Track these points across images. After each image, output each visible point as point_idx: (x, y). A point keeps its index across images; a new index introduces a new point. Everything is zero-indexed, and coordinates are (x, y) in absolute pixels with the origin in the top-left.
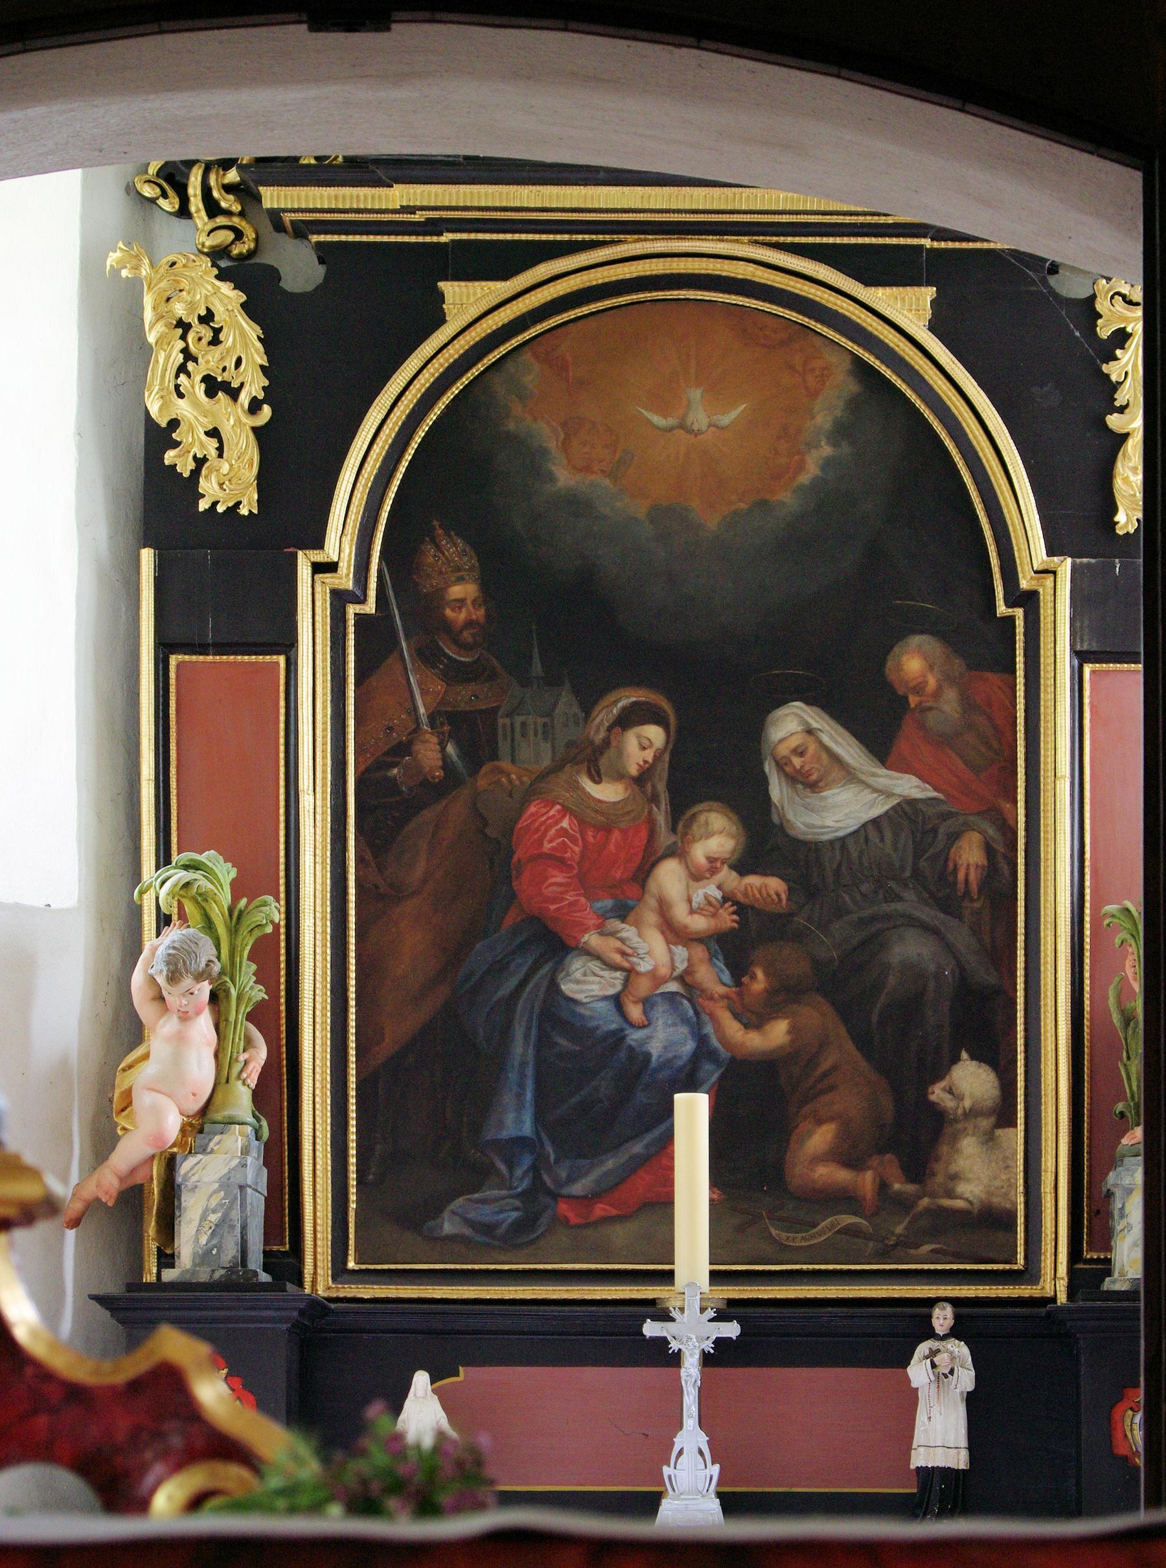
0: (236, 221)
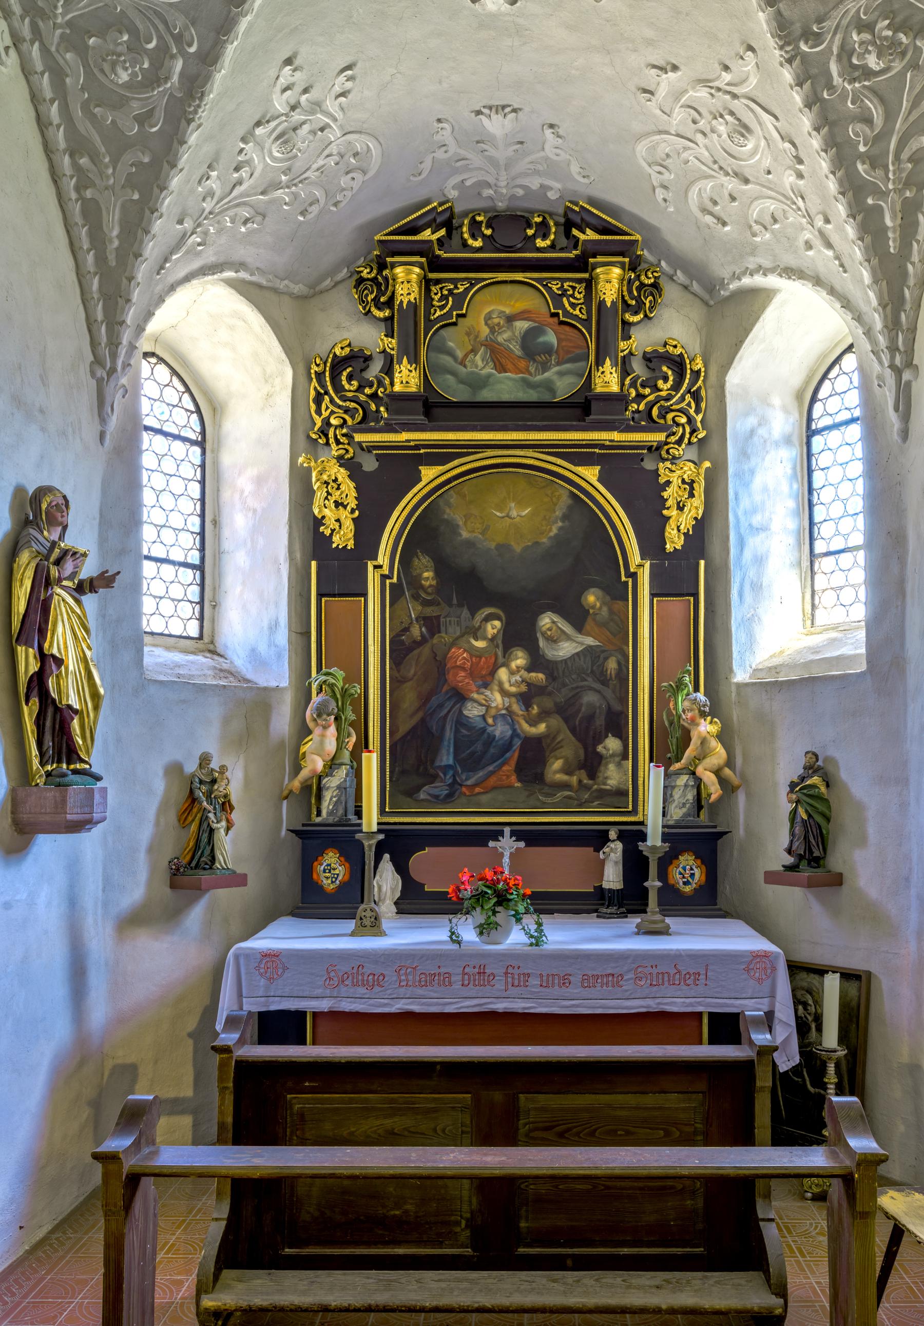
0: (346, 446)
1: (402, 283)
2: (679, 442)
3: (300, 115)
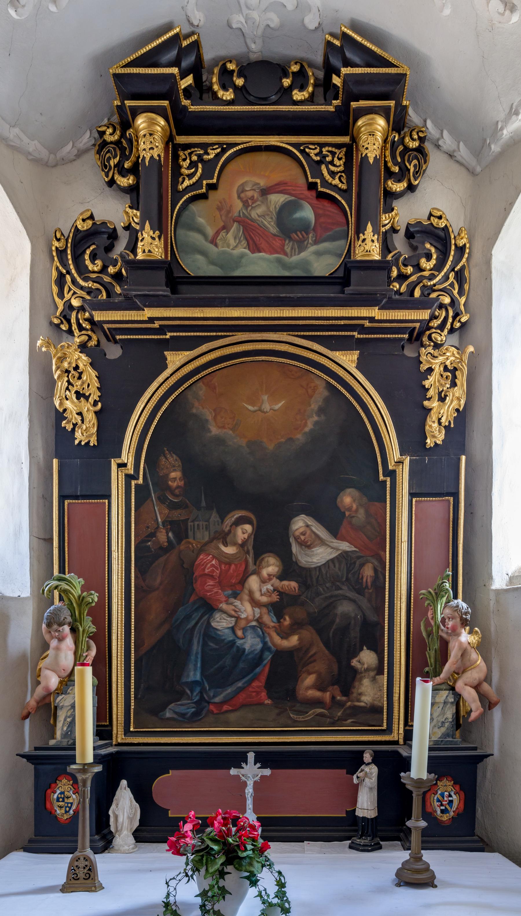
0: (89, 333)
1: (145, 136)
2: (441, 327)
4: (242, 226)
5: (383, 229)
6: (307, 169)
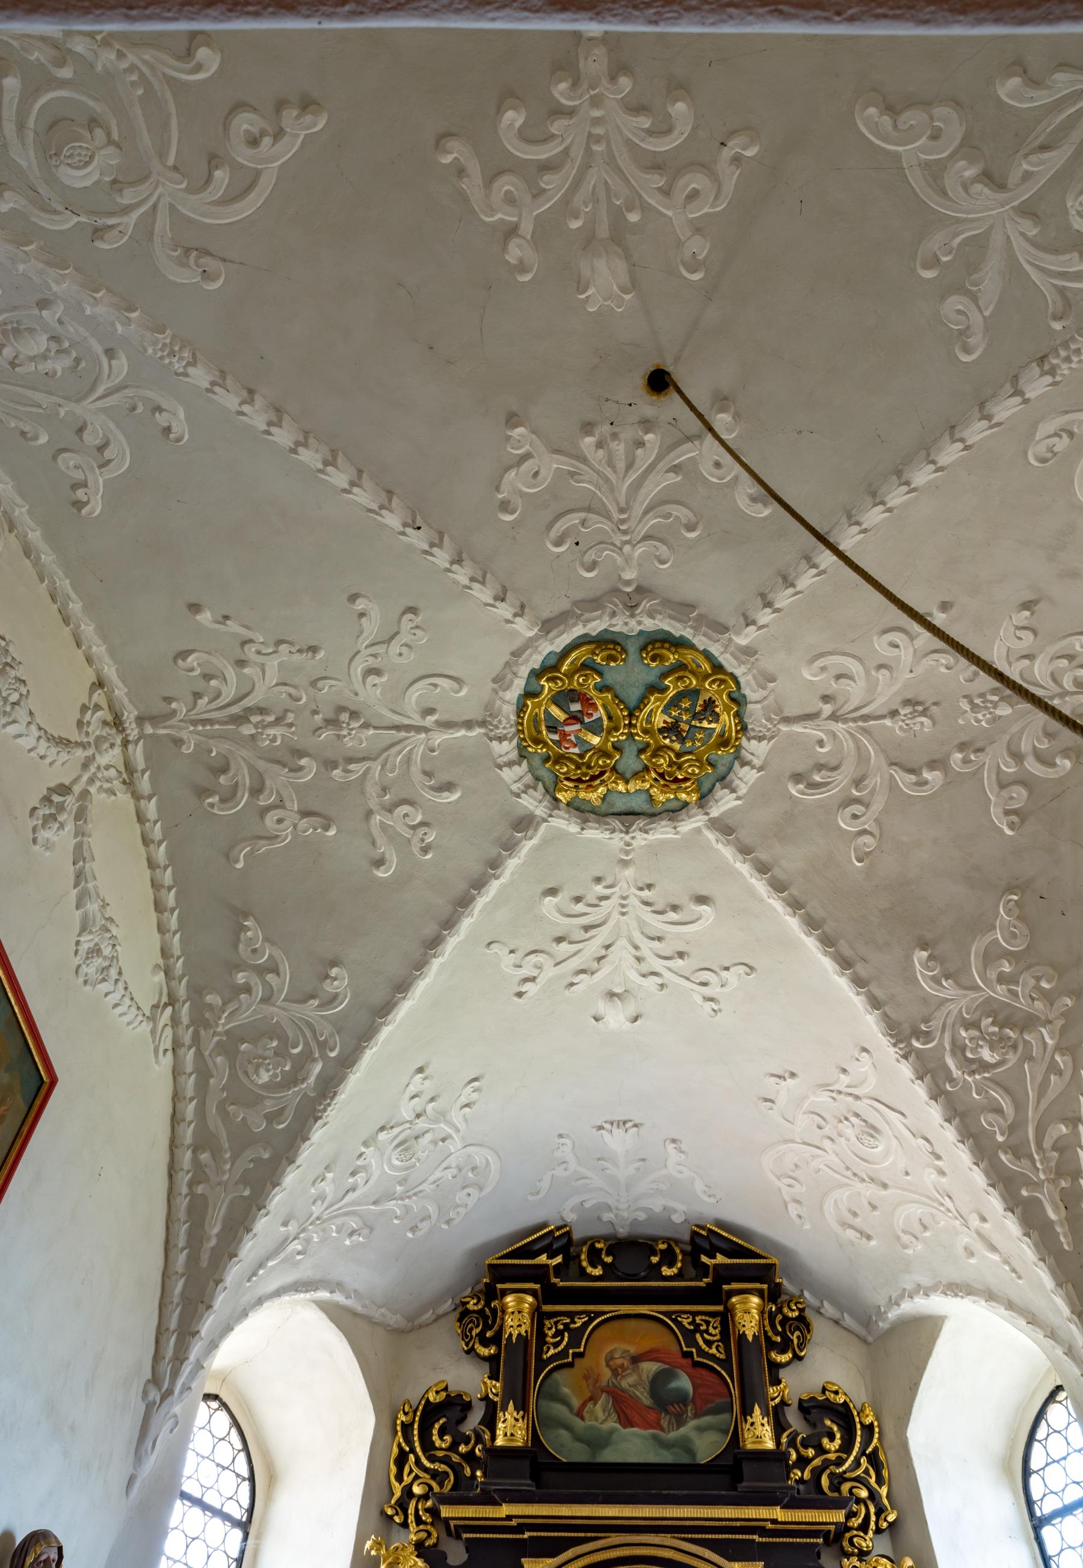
0: (429, 1527)
1: (513, 1313)
2: (864, 1527)
3: (425, 1123)
4: (613, 1397)
5: (772, 1403)
6: (681, 1337)
